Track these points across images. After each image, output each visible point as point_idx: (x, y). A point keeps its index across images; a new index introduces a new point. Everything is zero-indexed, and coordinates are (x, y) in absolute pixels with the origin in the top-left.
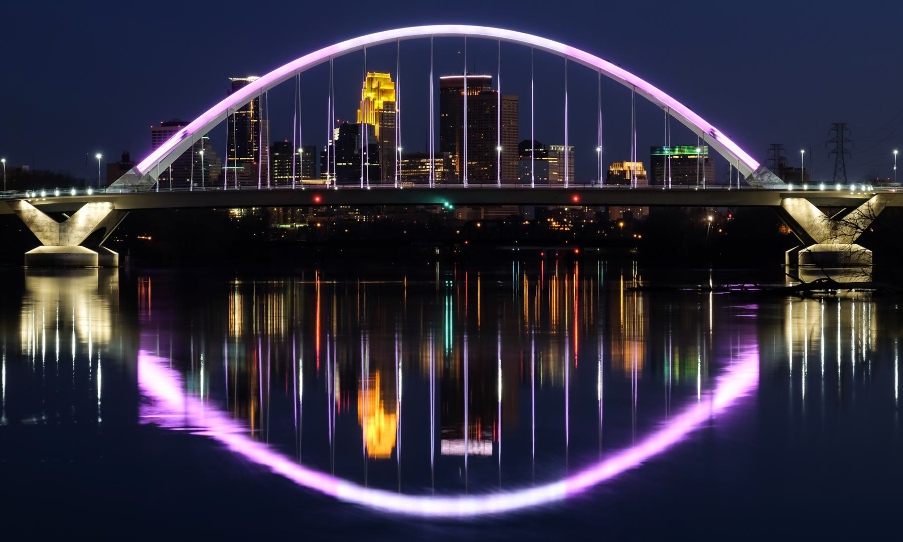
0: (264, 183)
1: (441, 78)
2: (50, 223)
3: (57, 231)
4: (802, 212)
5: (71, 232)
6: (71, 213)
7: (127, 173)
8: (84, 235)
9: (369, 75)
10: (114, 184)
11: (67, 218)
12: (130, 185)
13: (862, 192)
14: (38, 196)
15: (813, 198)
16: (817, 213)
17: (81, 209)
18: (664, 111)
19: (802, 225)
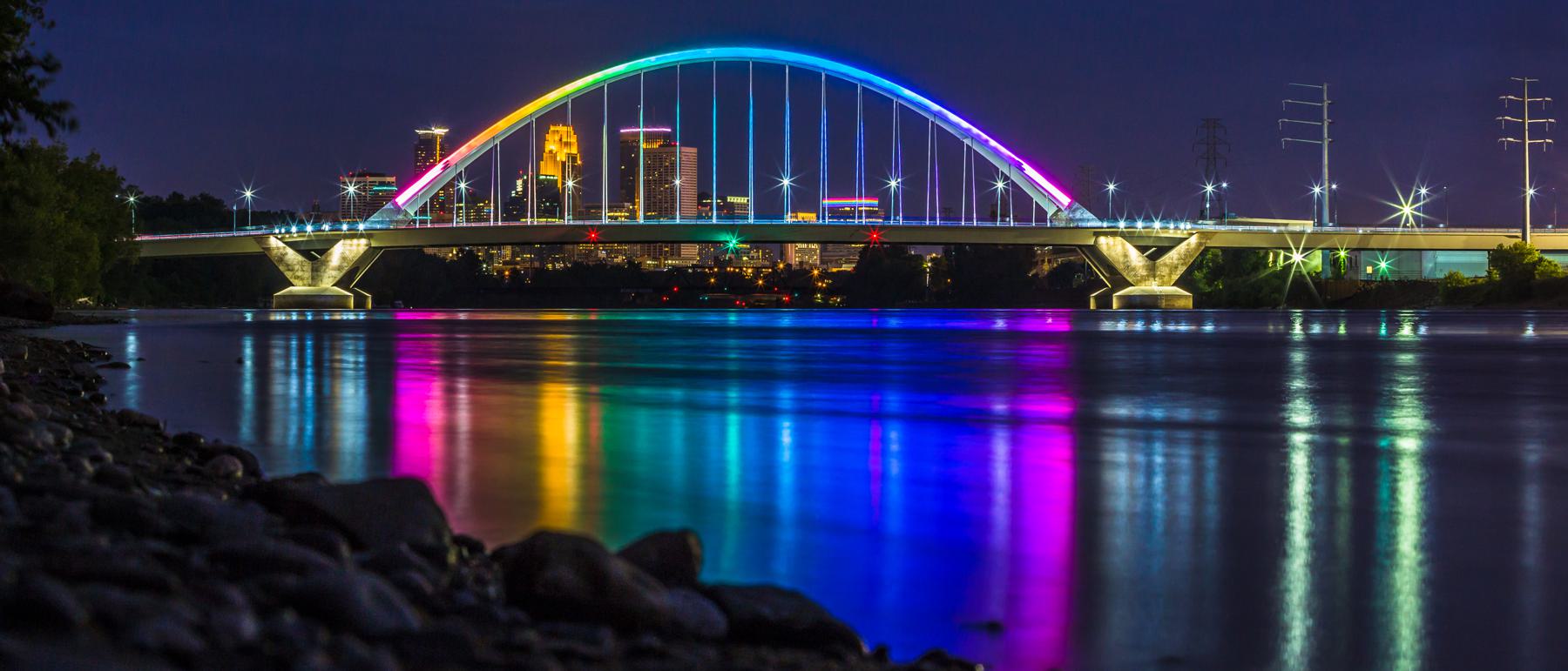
0: (496, 219)
1: (622, 131)
2: (302, 262)
3: (310, 270)
5: (325, 271)
6: (323, 252)
7: (385, 207)
8: (338, 275)
9: (552, 128)
10: (371, 219)
11: (318, 258)
14: (288, 232)
15: (1128, 236)
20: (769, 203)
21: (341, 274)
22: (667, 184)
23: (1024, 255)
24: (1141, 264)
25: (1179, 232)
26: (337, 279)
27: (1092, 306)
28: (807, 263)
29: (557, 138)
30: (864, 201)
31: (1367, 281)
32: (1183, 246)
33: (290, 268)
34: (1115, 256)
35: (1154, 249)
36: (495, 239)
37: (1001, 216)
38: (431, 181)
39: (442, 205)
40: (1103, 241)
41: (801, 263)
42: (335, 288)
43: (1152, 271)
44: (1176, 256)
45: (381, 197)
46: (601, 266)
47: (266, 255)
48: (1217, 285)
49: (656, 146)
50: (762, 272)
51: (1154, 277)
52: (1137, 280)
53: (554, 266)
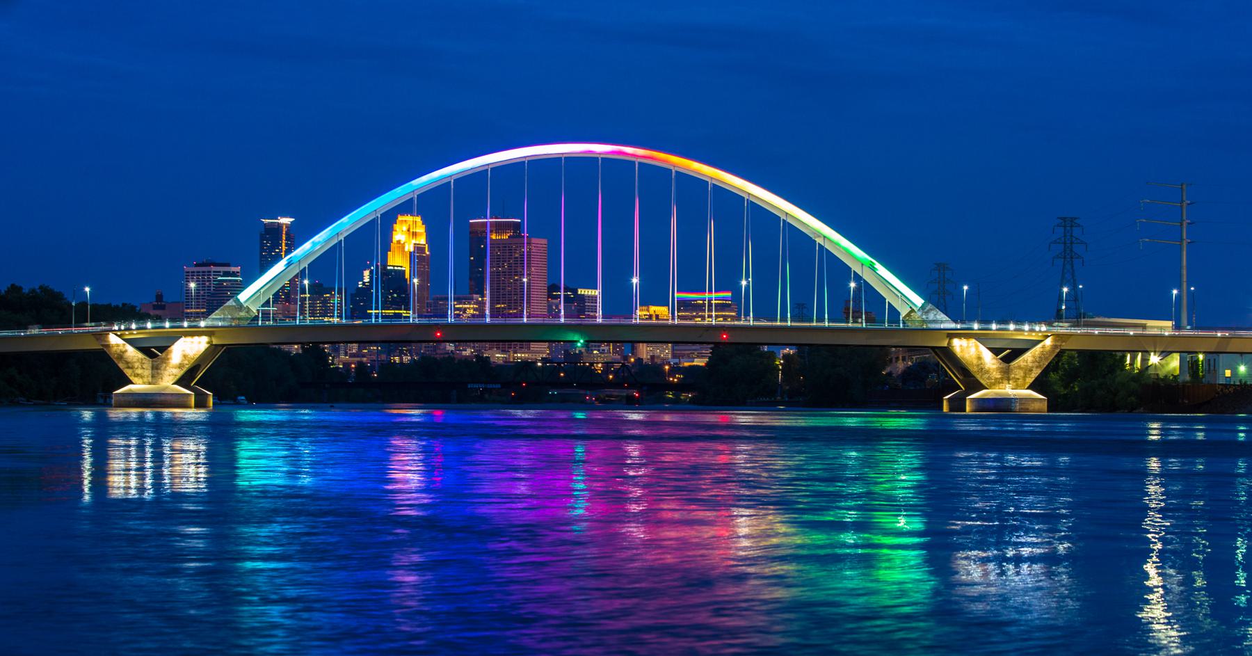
1: (471, 221)
2: (142, 359)
4: (971, 353)
5: (165, 370)
6: (163, 349)
7: (227, 304)
8: (179, 373)
10: (213, 316)
11: (158, 355)
12: (230, 317)
15: (979, 338)
17: (176, 344)
18: (815, 241)
20: (619, 301)
21: (182, 372)
22: (516, 275)
23: (881, 354)
24: (995, 367)
25: (1034, 334)
26: (178, 377)
27: (946, 408)
28: (659, 357)
29: (405, 228)
30: (714, 295)
31: (1225, 386)
32: (1038, 347)
33: (129, 365)
34: (968, 358)
35: (1008, 351)
36: (340, 336)
37: (853, 317)
38: (277, 275)
39: (288, 295)
40: (957, 343)
41: (653, 357)
42: (176, 386)
43: (1006, 375)
44: (1030, 359)
45: (225, 287)
46: (450, 358)
47: (105, 352)
48: (1073, 387)
49: (505, 237)
50: (613, 367)
51: (1009, 379)
52: (991, 383)
53: (401, 359)
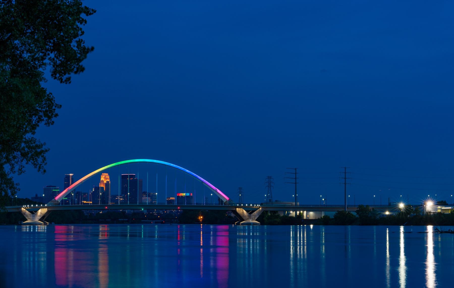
5: (36, 217)
8: (40, 218)
13: (258, 207)
15: (244, 208)
16: (245, 212)
19: (241, 215)
